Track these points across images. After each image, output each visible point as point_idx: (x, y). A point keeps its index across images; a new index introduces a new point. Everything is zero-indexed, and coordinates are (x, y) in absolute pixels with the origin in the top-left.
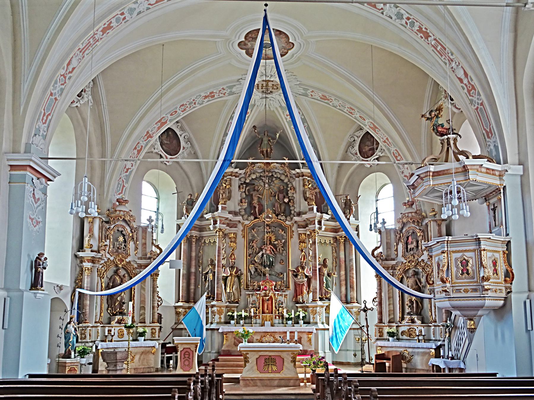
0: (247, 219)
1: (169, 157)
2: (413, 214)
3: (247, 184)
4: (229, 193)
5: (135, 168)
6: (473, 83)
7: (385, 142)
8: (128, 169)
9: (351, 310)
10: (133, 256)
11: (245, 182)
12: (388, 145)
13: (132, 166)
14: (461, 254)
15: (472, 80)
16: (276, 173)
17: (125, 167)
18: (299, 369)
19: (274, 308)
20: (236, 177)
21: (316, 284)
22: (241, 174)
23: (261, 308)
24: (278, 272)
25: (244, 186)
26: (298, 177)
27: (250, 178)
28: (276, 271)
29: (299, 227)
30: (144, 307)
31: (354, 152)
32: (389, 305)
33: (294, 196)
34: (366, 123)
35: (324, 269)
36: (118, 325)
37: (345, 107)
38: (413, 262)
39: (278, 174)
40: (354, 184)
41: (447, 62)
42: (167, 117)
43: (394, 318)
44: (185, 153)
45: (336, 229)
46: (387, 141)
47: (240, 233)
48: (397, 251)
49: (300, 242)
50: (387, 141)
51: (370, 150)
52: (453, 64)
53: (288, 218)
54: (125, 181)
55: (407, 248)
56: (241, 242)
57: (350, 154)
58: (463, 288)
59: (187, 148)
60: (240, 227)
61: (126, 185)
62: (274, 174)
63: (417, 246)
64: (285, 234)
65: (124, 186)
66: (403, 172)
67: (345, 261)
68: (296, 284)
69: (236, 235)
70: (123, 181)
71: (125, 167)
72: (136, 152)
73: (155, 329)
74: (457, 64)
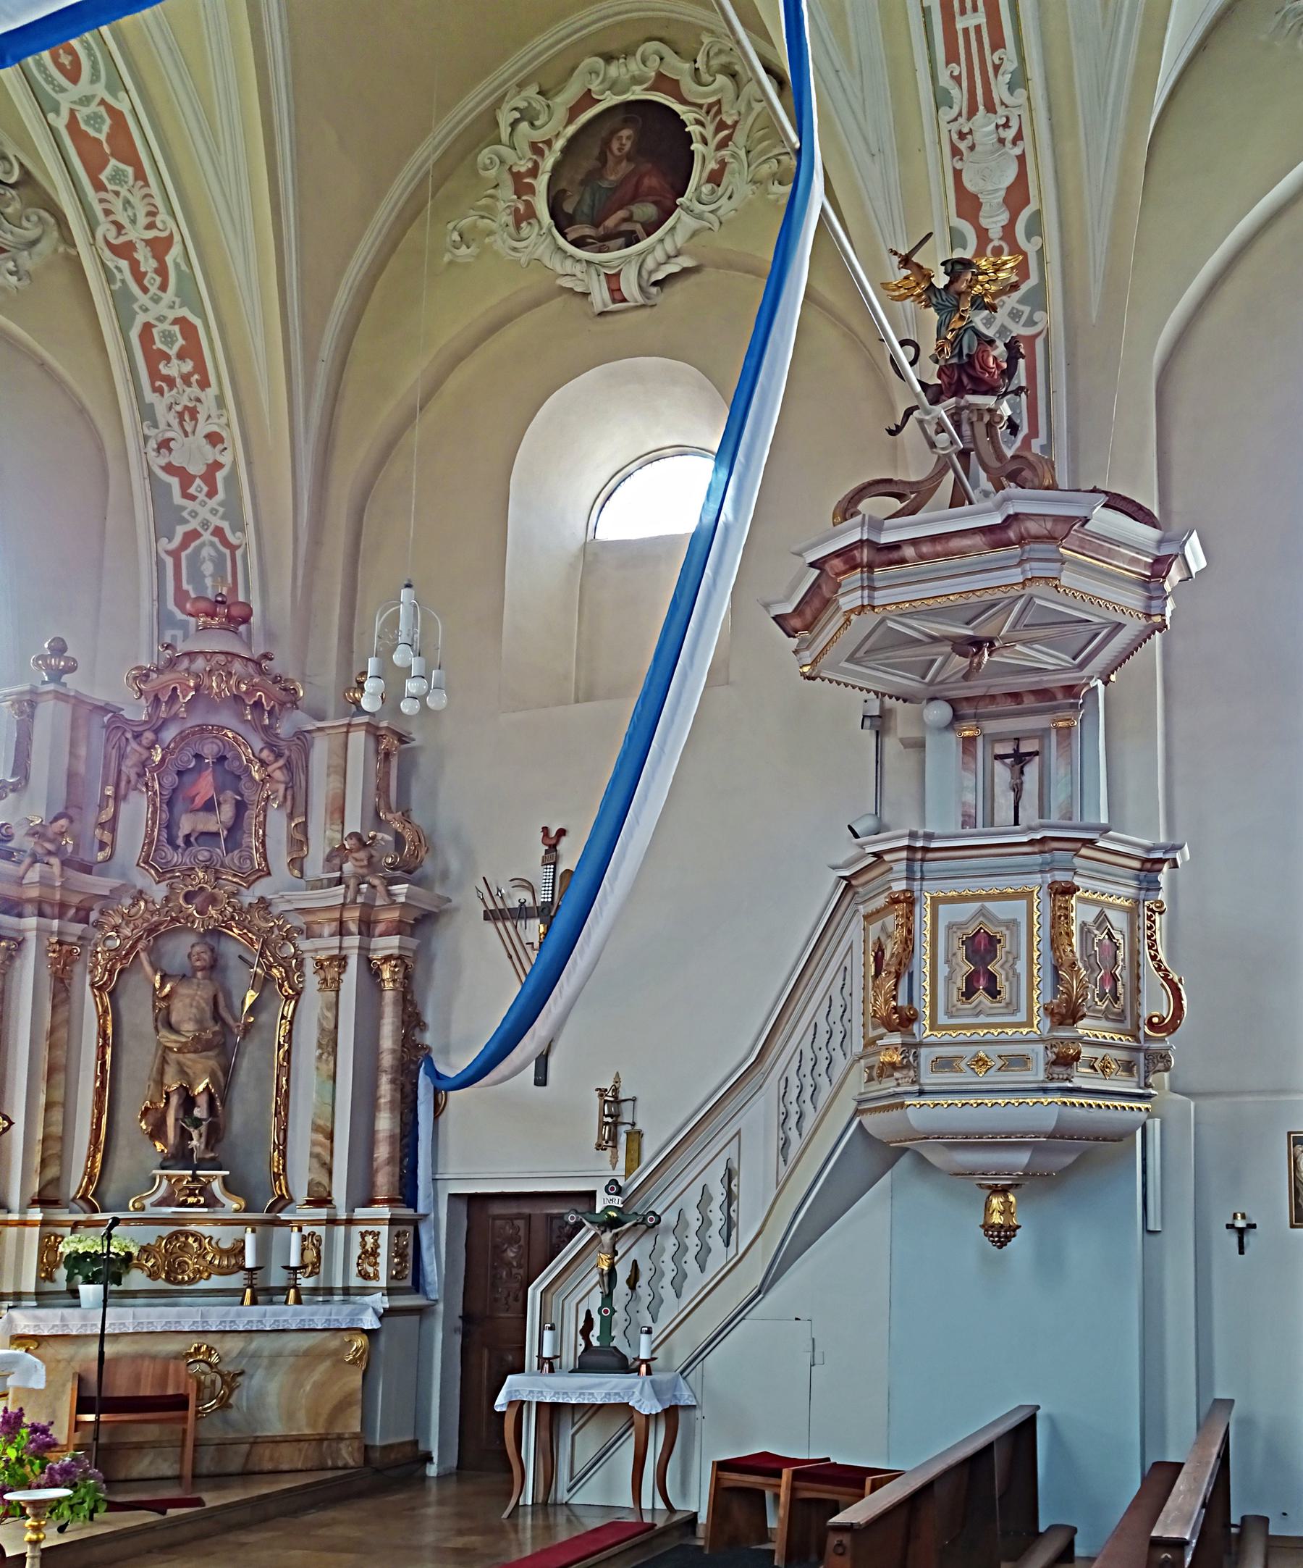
6: (1030, 247)
12: (139, 276)
14: (976, 906)
15: (1035, 228)
32: (49, 1106)
38: (213, 900)
41: (959, 97)
42: (86, 101)
43: (56, 1182)
48: (113, 831)
50: (142, 254)
52: (984, 126)
55: (170, 826)
58: (968, 1051)
63: (235, 828)
66: (165, 445)
74: (1010, 134)
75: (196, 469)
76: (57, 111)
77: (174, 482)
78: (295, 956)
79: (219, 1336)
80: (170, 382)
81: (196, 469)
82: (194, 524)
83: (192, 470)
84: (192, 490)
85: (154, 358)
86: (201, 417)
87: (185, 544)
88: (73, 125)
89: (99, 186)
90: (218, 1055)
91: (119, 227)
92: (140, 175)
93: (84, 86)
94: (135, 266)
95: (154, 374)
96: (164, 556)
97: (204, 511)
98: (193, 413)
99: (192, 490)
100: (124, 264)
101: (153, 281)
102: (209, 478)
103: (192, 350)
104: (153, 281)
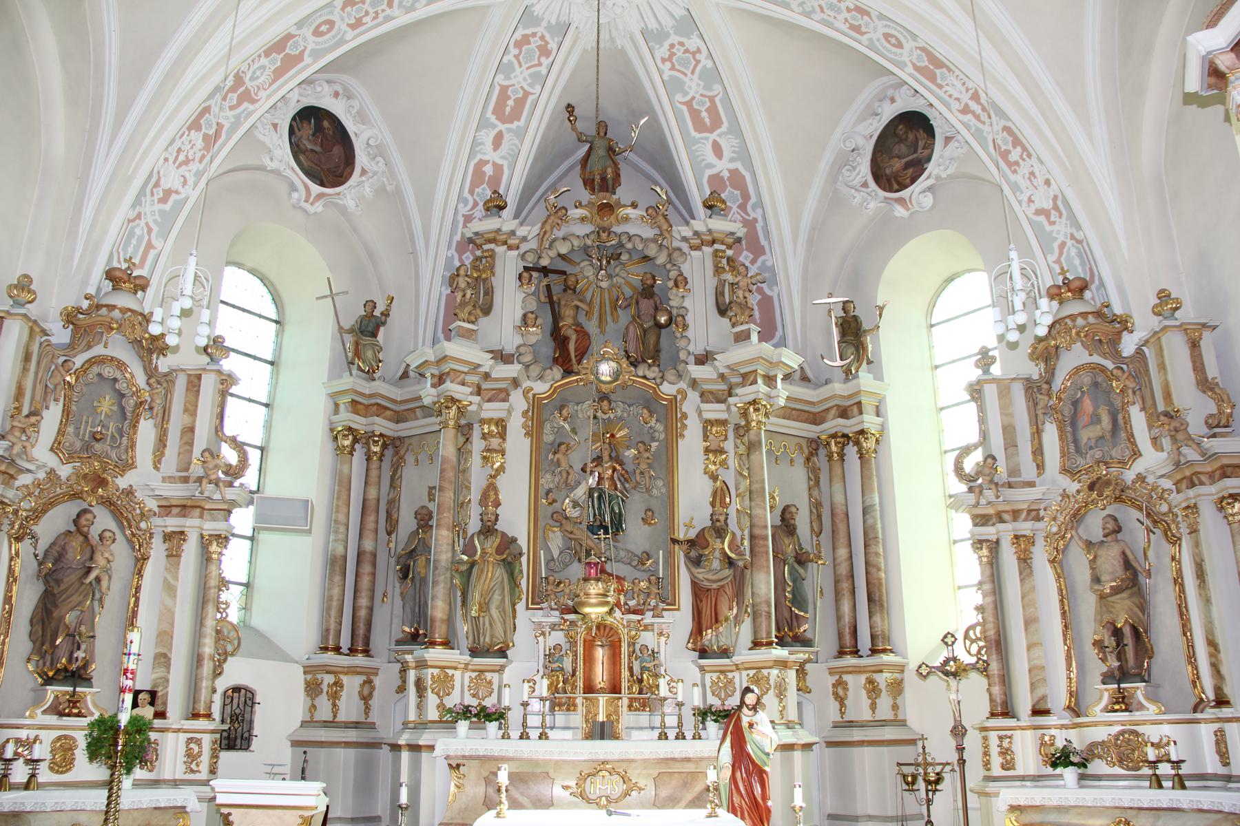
0: (541, 378)
1: (316, 189)
2: (1091, 319)
3: (545, 271)
4: (486, 294)
5: (193, 194)
7: (965, 110)
8: (168, 193)
9: (877, 677)
12: (977, 117)
13: (185, 183)
16: (630, 238)
17: (157, 184)
18: (342, 703)
19: (625, 674)
20: (510, 248)
21: (764, 584)
22: (524, 239)
23: (580, 673)
24: (639, 552)
26: (697, 248)
27: (553, 253)
28: (632, 547)
29: (705, 396)
30: (165, 656)
31: (858, 181)
33: (687, 303)
34: (906, 59)
35: (786, 541)
36: (53, 720)
37: (839, 11)
39: (637, 240)
40: (862, 267)
42: (305, 39)
44: (366, 185)
45: (814, 414)
46: (974, 106)
47: (516, 425)
50: (974, 106)
51: (907, 166)
53: (670, 375)
54: (155, 229)
56: (518, 446)
57: (845, 190)
59: (375, 173)
60: (518, 402)
61: (157, 243)
62: (624, 239)
65: (150, 246)
66: (1030, 201)
68: (698, 591)
69: (504, 427)
70: (150, 230)
71: (157, 184)
72: (197, 138)
73: (199, 742)
75: (1048, 205)
76: (906, 65)
77: (1042, 219)
78: (1170, 511)
79: (1135, 812)
80: (1017, 163)
81: (1048, 205)
82: (1061, 238)
83: (1045, 206)
84: (1052, 219)
85: (1005, 155)
86: (1037, 174)
87: (1061, 254)
88: (915, 67)
89: (940, 87)
90: (1131, 596)
91: (958, 99)
92: (949, 70)
93: (311, 39)
94: (973, 113)
95: (1009, 164)
96: (1052, 265)
97: (1061, 229)
98: (1032, 173)
99: (1052, 219)
100: (970, 116)
101: (984, 117)
102: (1056, 208)
103: (1017, 142)
104: (984, 117)
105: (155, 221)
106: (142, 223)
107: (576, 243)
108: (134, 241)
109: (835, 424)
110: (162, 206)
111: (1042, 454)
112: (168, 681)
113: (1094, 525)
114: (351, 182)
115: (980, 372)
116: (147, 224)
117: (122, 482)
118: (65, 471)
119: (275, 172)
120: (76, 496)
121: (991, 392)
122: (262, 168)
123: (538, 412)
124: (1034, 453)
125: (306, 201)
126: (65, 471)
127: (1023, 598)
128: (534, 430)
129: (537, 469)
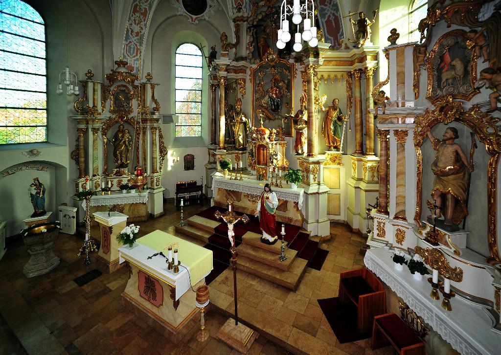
0: (254, 63)
1: (194, 17)
10: (135, 111)
11: (253, 25)
17: (132, 31)
25: (252, 29)
47: (248, 78)
49: (303, 81)
56: (249, 86)
60: (248, 72)
64: (289, 74)
67: (361, 101)
70: (136, 45)
105: (137, 42)
106: (133, 43)
107: (264, 14)
108: (132, 49)
109: (357, 66)
110: (137, 37)
111: (418, 87)
112: (404, 73)
113: (442, 130)
114: (206, 11)
115: (390, 43)
116: (134, 43)
117: (130, 116)
118: (114, 116)
119: (181, 15)
120: (117, 122)
121: (393, 53)
122: (176, 15)
123: (254, 73)
124: (414, 86)
125: (192, 21)
126: (114, 116)
127: (397, 162)
128: (254, 80)
129: (255, 92)
